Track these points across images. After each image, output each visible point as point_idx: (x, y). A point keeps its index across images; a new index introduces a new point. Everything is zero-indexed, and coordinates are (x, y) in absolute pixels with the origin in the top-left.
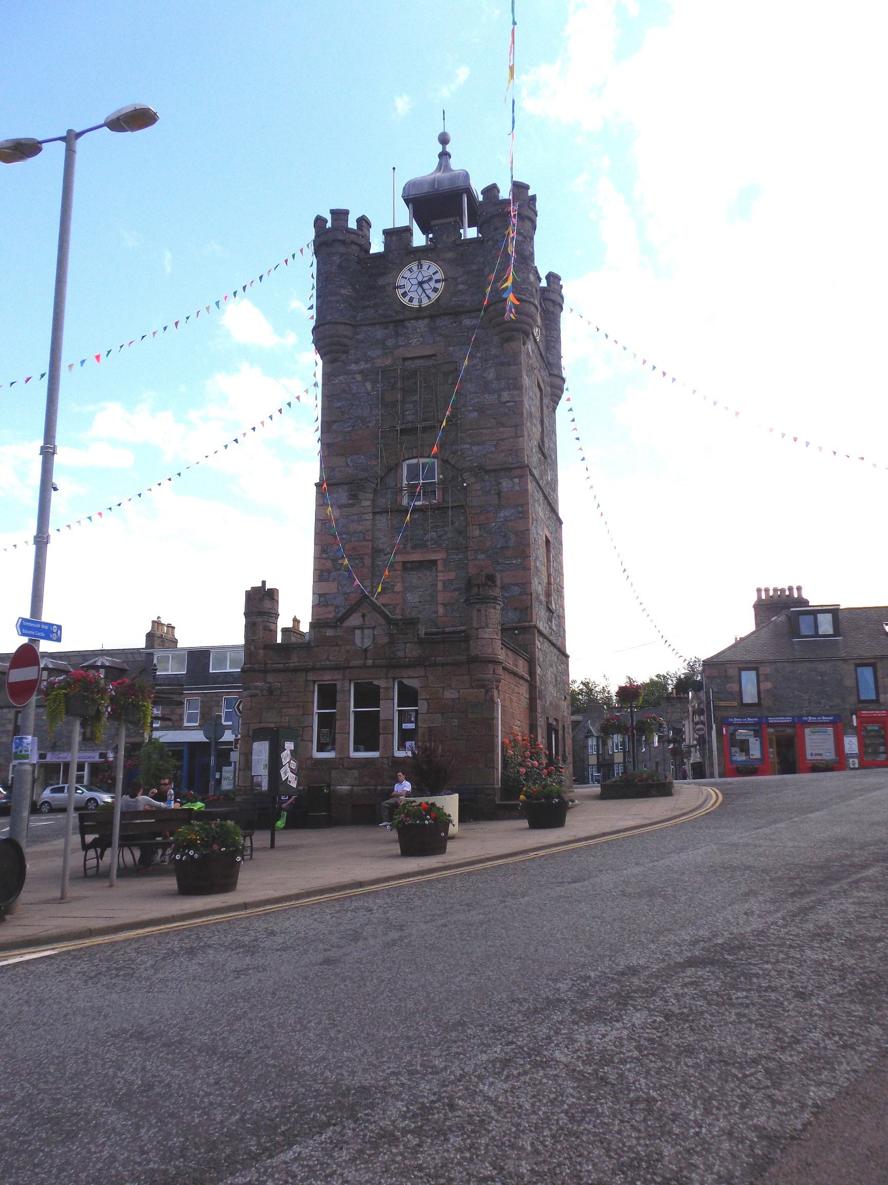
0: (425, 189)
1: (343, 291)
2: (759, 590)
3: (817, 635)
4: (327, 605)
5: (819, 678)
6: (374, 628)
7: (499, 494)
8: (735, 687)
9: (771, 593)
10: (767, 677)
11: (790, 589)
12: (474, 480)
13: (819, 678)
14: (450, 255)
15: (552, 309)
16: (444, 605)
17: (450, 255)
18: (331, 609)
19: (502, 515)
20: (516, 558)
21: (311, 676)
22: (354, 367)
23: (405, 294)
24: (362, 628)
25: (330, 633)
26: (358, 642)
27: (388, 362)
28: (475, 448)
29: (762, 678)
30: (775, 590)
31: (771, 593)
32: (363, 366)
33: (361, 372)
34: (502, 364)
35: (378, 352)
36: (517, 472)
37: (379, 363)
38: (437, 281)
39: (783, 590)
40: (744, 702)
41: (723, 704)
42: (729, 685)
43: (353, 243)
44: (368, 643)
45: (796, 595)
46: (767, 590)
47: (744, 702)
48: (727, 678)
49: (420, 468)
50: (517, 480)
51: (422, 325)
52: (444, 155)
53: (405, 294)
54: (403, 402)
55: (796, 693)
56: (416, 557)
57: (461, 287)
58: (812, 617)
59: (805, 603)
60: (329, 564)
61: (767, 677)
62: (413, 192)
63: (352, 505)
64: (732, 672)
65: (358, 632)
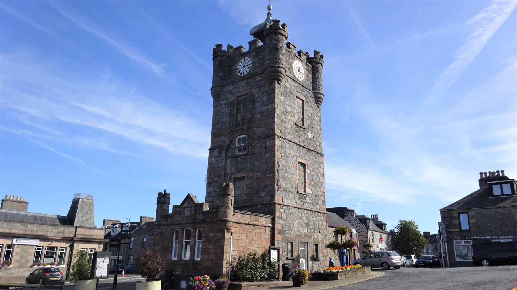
0: (257, 29)
1: (219, 74)
2: (481, 174)
3: (503, 194)
4: (210, 197)
5: (501, 217)
6: (191, 207)
7: (266, 147)
8: (457, 222)
9: (488, 175)
10: (473, 217)
11: (498, 172)
12: (257, 142)
13: (501, 217)
14: (254, 54)
15: (315, 66)
16: (246, 195)
17: (254, 54)
18: (211, 198)
19: (266, 156)
20: (270, 173)
21: (173, 227)
22: (223, 103)
23: (239, 72)
24: (187, 208)
25: (178, 209)
26: (186, 213)
27: (233, 99)
28: (259, 129)
29: (470, 217)
30: (490, 173)
31: (488, 175)
32: (225, 101)
33: (225, 104)
34: (269, 94)
35: (230, 96)
36: (272, 138)
37: (230, 100)
38: (250, 65)
39: (494, 173)
40: (462, 229)
41: (451, 230)
42: (453, 221)
43: (223, 55)
44: (189, 213)
45: (501, 175)
46: (485, 173)
47: (462, 229)
48: (452, 218)
49: (239, 140)
50: (272, 141)
51: (244, 83)
52: (269, 14)
53: (239, 72)
54: (237, 114)
55: (489, 224)
56: (238, 175)
57: (257, 65)
58: (499, 185)
59: (506, 178)
60: (211, 180)
61: (473, 217)
62: (254, 31)
63: (219, 156)
64: (455, 214)
65: (186, 209)
